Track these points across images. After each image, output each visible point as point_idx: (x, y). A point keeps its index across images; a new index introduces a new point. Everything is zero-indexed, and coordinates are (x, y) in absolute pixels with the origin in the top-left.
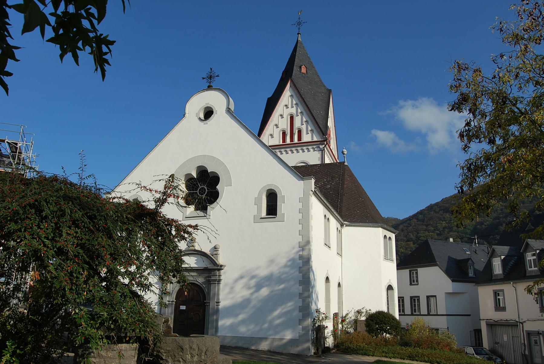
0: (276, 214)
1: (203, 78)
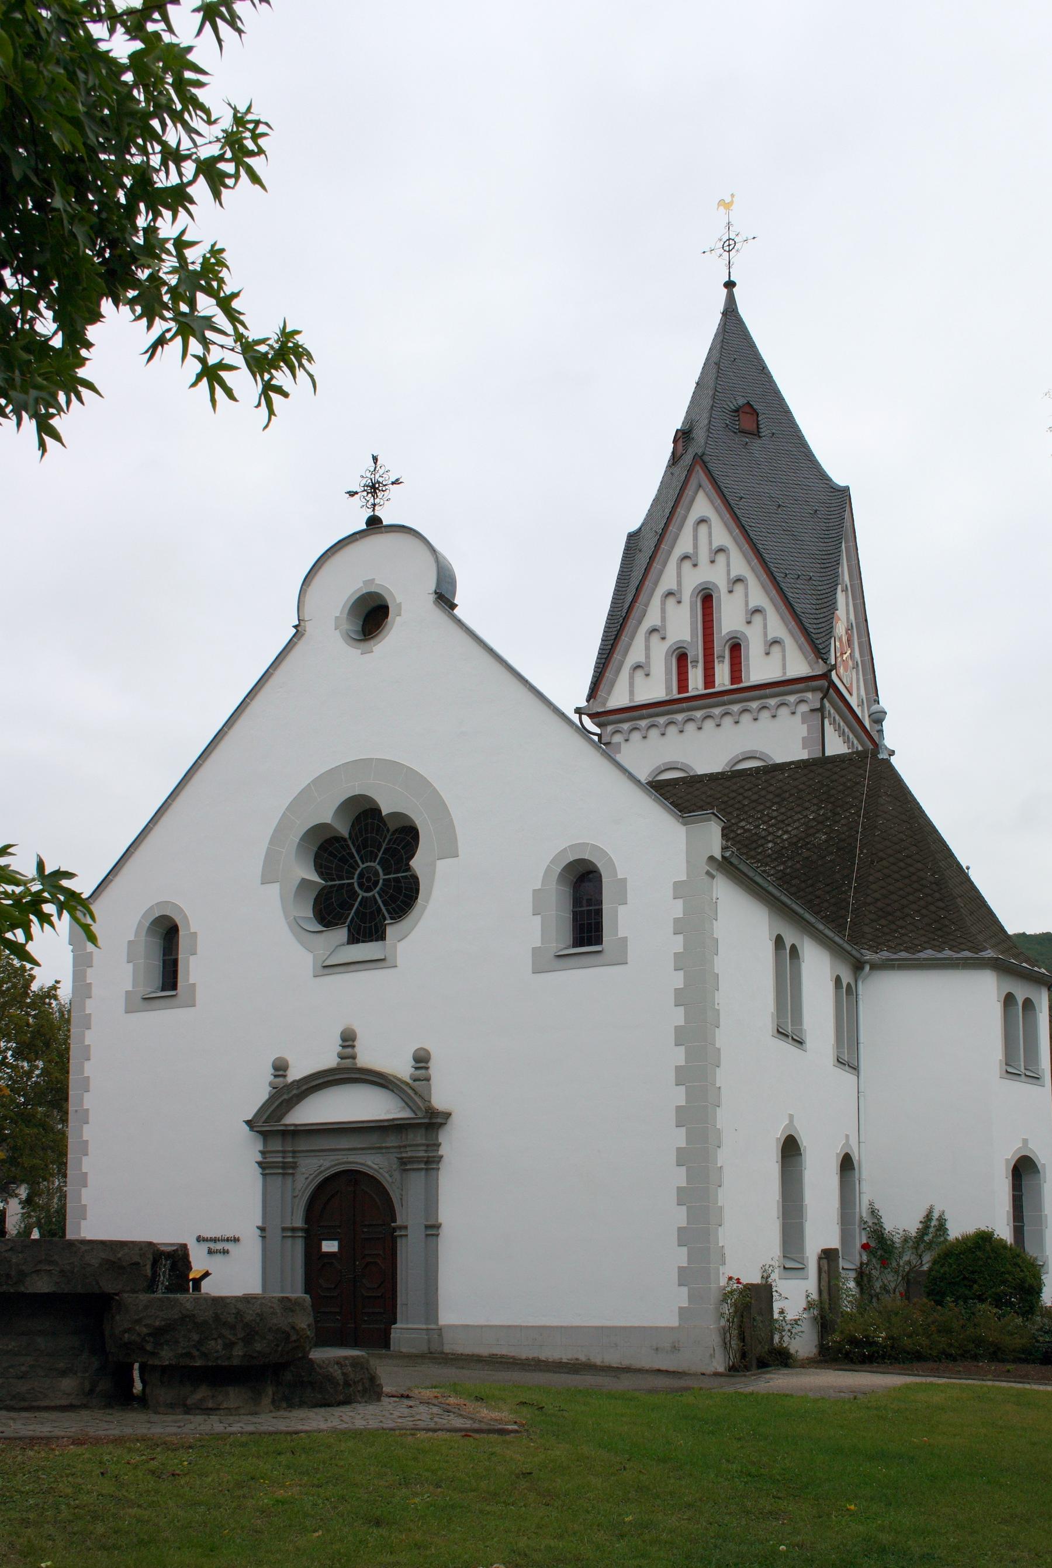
0: (599, 941)
1: (352, 494)
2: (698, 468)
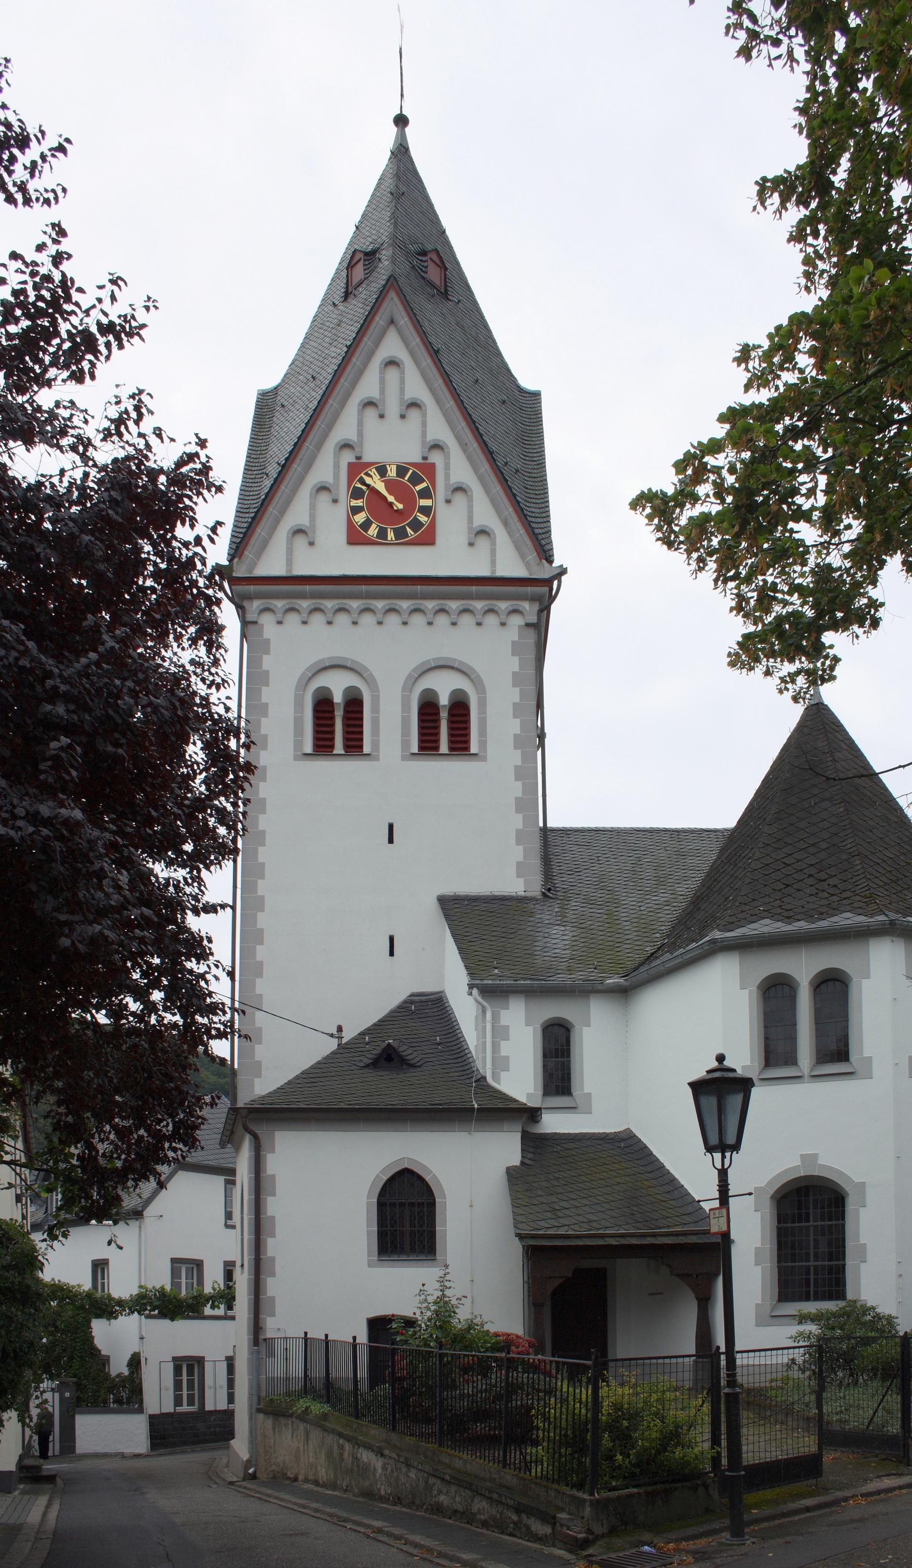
2: (392, 294)
